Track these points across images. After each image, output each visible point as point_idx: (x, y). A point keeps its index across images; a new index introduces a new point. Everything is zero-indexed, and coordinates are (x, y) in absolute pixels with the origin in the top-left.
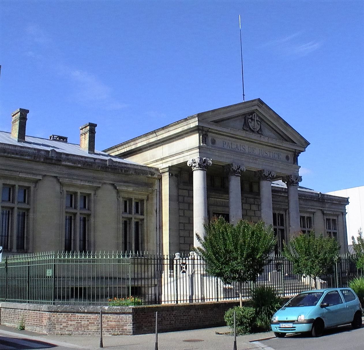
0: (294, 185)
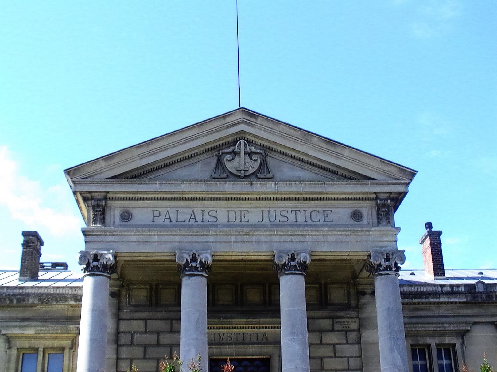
0: (381, 275)
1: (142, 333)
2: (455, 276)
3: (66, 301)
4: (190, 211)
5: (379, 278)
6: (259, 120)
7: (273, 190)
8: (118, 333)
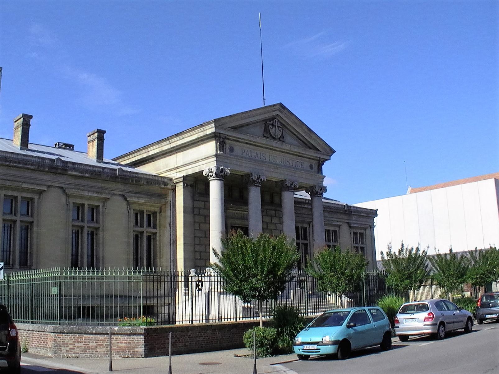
1: (203, 208)
2: (48, 152)
3: (160, 185)
4: (256, 152)
5: (317, 198)
6: (285, 111)
7: (288, 149)
8: (194, 208)
